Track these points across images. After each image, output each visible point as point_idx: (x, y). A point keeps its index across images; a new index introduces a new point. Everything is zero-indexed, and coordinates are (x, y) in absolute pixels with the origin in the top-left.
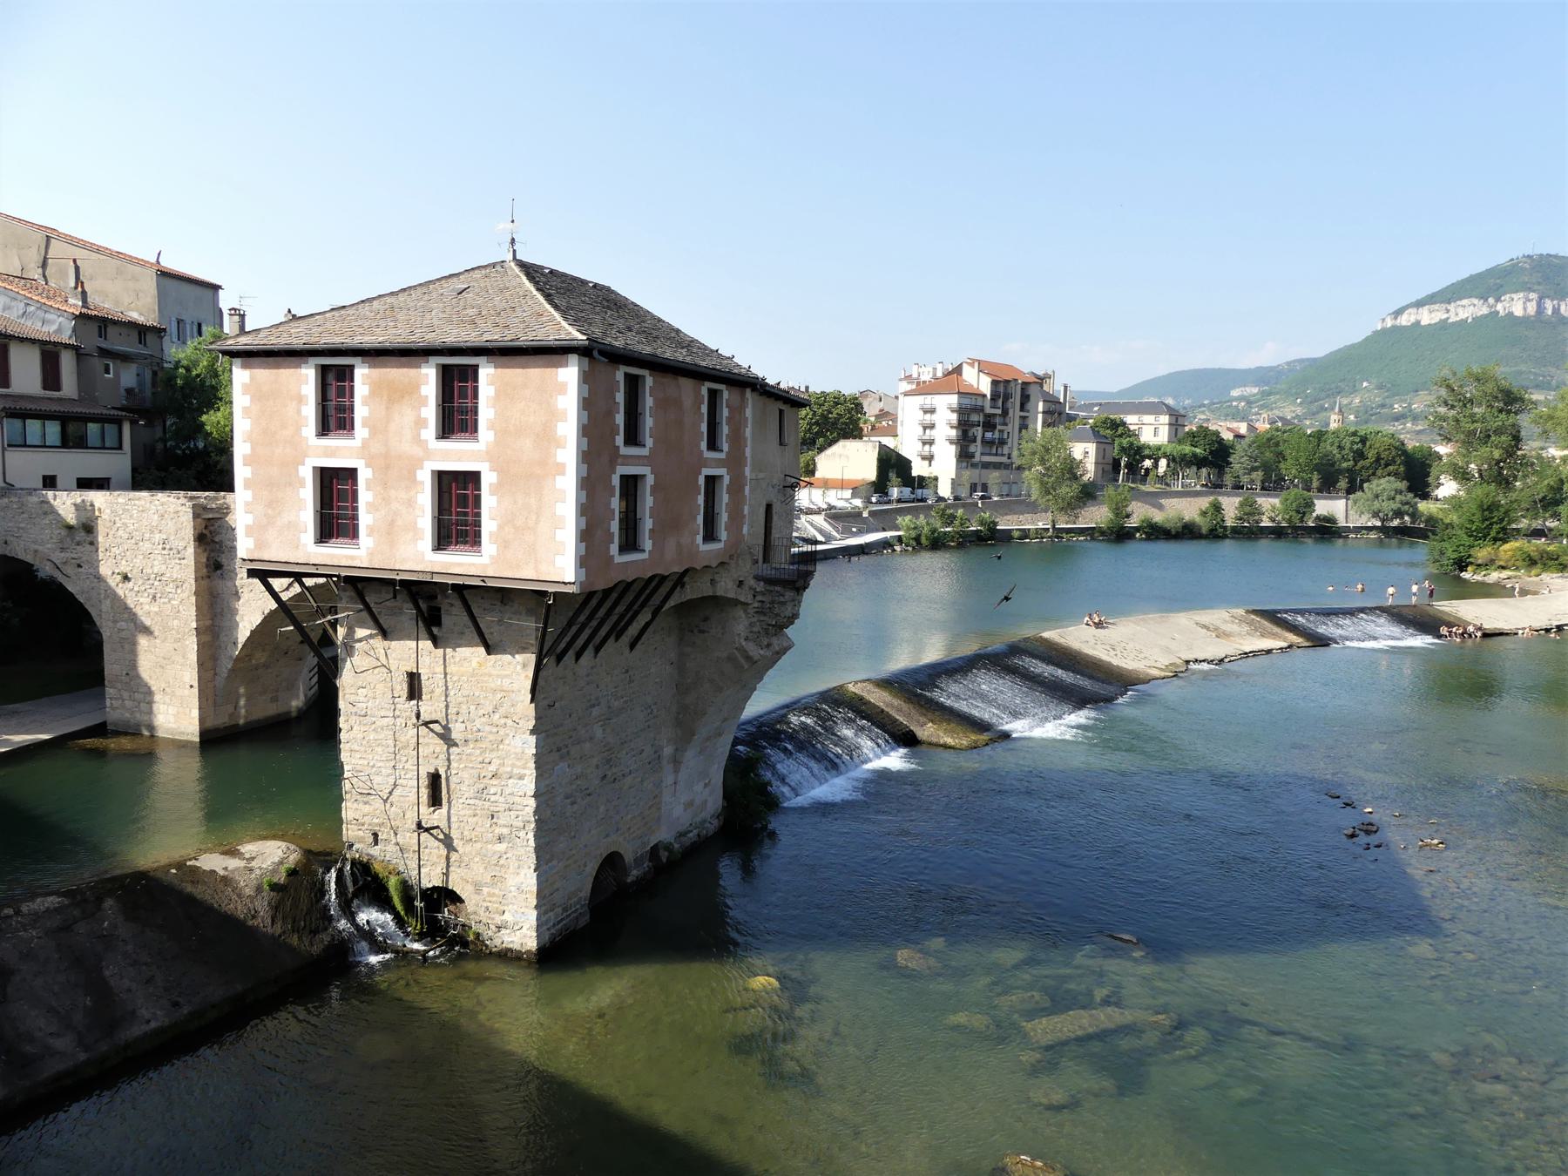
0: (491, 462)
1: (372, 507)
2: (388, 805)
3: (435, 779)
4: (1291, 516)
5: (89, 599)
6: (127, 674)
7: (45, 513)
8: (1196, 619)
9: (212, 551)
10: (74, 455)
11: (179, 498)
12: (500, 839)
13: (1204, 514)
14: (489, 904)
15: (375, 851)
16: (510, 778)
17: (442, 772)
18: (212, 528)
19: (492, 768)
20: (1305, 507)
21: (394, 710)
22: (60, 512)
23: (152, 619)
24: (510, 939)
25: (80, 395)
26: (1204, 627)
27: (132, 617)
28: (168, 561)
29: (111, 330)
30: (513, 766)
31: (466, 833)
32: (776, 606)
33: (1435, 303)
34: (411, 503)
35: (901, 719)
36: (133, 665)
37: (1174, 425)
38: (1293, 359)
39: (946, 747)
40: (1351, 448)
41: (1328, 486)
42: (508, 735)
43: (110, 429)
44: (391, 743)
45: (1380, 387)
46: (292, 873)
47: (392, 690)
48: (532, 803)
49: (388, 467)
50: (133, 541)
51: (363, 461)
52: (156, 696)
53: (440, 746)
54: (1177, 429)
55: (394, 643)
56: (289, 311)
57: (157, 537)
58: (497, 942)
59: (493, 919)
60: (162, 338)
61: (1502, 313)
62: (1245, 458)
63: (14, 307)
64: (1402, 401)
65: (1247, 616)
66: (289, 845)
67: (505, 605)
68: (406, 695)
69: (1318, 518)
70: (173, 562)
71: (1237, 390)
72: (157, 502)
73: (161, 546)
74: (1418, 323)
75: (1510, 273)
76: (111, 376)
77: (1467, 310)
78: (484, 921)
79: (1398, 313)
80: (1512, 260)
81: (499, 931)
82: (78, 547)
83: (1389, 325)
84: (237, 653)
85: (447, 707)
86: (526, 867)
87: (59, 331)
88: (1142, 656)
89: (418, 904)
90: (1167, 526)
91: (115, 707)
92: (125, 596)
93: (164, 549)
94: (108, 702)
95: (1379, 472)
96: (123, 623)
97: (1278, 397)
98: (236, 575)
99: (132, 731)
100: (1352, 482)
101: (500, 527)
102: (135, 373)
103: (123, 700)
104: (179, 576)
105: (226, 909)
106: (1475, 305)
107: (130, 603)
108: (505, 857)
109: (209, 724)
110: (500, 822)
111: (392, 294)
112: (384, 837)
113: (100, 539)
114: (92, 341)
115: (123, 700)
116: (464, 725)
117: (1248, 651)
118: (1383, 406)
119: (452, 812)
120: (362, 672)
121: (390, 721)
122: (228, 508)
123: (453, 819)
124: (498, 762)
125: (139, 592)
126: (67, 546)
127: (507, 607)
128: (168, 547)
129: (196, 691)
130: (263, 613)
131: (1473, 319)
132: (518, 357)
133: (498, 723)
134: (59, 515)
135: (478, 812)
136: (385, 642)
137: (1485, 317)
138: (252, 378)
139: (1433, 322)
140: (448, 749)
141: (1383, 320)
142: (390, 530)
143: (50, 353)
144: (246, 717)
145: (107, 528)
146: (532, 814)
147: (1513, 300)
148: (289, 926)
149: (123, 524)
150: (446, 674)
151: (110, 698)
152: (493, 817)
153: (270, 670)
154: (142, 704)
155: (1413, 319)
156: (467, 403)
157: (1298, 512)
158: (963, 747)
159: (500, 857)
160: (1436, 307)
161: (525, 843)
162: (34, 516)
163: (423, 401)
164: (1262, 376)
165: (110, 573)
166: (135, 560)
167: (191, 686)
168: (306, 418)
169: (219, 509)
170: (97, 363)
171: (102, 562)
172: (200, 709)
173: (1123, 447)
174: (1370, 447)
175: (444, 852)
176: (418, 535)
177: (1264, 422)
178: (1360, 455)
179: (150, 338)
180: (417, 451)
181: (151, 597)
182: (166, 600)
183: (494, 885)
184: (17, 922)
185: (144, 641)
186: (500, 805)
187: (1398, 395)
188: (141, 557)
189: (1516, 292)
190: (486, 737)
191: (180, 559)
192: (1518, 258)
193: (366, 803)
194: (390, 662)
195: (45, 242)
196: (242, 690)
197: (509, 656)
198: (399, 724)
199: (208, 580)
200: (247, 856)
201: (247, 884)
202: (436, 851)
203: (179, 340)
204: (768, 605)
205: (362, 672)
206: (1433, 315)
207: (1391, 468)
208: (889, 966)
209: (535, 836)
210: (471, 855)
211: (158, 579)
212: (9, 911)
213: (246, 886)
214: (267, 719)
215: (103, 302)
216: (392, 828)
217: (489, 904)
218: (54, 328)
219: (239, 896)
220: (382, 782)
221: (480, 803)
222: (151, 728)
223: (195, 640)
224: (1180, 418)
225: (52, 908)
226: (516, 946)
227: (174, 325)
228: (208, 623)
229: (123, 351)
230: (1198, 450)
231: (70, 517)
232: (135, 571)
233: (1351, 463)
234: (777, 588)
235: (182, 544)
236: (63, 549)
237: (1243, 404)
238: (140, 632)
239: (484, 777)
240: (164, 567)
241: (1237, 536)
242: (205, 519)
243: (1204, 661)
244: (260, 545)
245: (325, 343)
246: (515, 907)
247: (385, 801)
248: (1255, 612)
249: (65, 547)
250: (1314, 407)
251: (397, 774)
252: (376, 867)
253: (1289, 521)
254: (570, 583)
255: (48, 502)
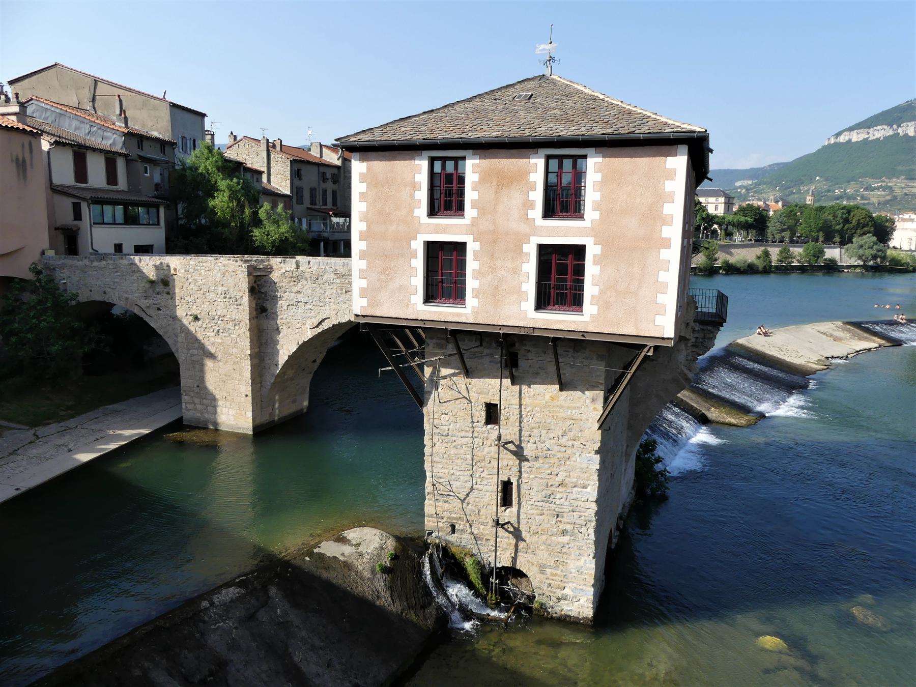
0: (594, 237)
1: (478, 274)
2: (465, 505)
3: (506, 487)
4: (810, 260)
5: (166, 333)
6: (198, 386)
7: (134, 272)
8: (817, 329)
9: (259, 299)
10: (109, 229)
11: (237, 261)
12: (563, 533)
13: (759, 258)
14: (551, 582)
15: (453, 538)
16: (575, 487)
17: (514, 481)
18: (259, 283)
19: (559, 479)
20: (819, 253)
21: (473, 432)
22: (144, 271)
23: (217, 348)
24: (569, 608)
25: (128, 188)
26: (824, 334)
27: (202, 347)
28: (228, 307)
29: (146, 144)
30: (578, 477)
31: (533, 527)
32: (706, 341)
33: (861, 128)
34: (516, 271)
35: (695, 405)
36: (202, 379)
37: (727, 203)
38: (772, 163)
39: (730, 425)
40: (841, 217)
41: (829, 239)
42: (575, 454)
43: (153, 210)
44: (469, 457)
45: (826, 180)
46: (395, 558)
47: (472, 417)
48: (594, 507)
49: (495, 242)
50: (202, 292)
51: (472, 237)
52: (219, 402)
53: (513, 461)
54: (729, 206)
55: (474, 381)
56: (232, 133)
57: (220, 289)
58: (557, 609)
59: (555, 593)
60: (174, 149)
61: (901, 134)
62: (778, 223)
63: (82, 128)
64: (840, 188)
65: (844, 326)
66: (382, 532)
67: (577, 352)
68: (484, 421)
69: (826, 260)
70: (232, 307)
71: (739, 182)
72: (220, 264)
73: (223, 296)
74: (850, 140)
75: (906, 110)
76: (148, 175)
77: (880, 132)
78: (547, 593)
79: (838, 135)
80: (908, 102)
81: (559, 602)
82: (157, 296)
83: (832, 142)
84: (278, 371)
85: (521, 430)
86: (586, 555)
87: (113, 144)
88: (799, 354)
89: (493, 580)
90: (738, 266)
91: (189, 410)
92: (196, 331)
93: (226, 298)
94: (184, 405)
95: (858, 231)
96: (194, 350)
97: (765, 186)
98: (277, 316)
99: (200, 426)
100: (842, 237)
101: (602, 292)
102: (159, 174)
103: (195, 404)
104: (237, 318)
105: (357, 591)
106: (885, 130)
107: (200, 336)
108: (567, 547)
109: (258, 422)
110: (563, 520)
111: (466, 100)
112: (461, 527)
113: (177, 290)
114: (135, 152)
115: (195, 404)
116: (535, 445)
117: (858, 350)
118: (829, 191)
119: (521, 511)
120: (445, 402)
121: (470, 440)
122: (271, 268)
123: (521, 517)
124: (565, 474)
125: (206, 328)
126: (150, 295)
127: (579, 354)
128: (228, 296)
129: (250, 398)
130: (298, 344)
131: (884, 138)
132: (664, 147)
133: (566, 444)
134: (144, 273)
135: (544, 512)
136: (467, 379)
137: (891, 136)
138: (368, 168)
139: (859, 140)
140: (520, 464)
141: (829, 139)
142: (495, 294)
143: (110, 158)
144: (279, 415)
145: (182, 283)
146: (593, 515)
147: (908, 126)
148: (405, 603)
149: (194, 279)
150: (520, 405)
151: (185, 403)
152: (558, 516)
153: (294, 381)
154: (208, 408)
155: (847, 138)
156: (452, 187)
157: (814, 256)
158: (743, 425)
159: (562, 547)
160: (861, 131)
161: (586, 537)
162: (125, 274)
163: (533, 187)
164: (753, 173)
165: (184, 315)
166: (202, 306)
167: (246, 396)
168: (419, 201)
169: (265, 269)
170: (140, 166)
171: (178, 307)
172: (253, 411)
173: (703, 217)
174: (853, 216)
175: (513, 541)
176: (522, 296)
177: (771, 201)
178: (846, 221)
179: (167, 149)
180: (523, 228)
181: (215, 332)
182: (227, 334)
183: (556, 567)
184: (215, 613)
185: (210, 363)
186: (565, 507)
187: (837, 184)
188: (208, 303)
189: (910, 121)
190: (554, 455)
191: (237, 305)
192: (911, 101)
193: (446, 502)
194: (471, 395)
195: (93, 84)
196: (277, 397)
197: (579, 393)
198: (476, 443)
199: (256, 320)
200: (354, 543)
201: (363, 566)
202: (506, 540)
203: (183, 150)
204: (701, 340)
205: (445, 402)
206: (859, 136)
207: (866, 229)
208: (847, 621)
209: (595, 532)
210: (537, 544)
211: (221, 319)
212: (205, 604)
213: (363, 569)
214: (291, 415)
215: (134, 125)
216: (468, 521)
217: (551, 582)
218: (110, 142)
219: (361, 578)
220: (461, 486)
221: (547, 505)
222: (216, 424)
223: (250, 363)
224: (731, 199)
225: (234, 598)
226: (573, 614)
227: (180, 140)
228: (257, 350)
229: (155, 158)
230: (749, 219)
231: (152, 274)
232: (203, 314)
233: (841, 226)
234: (709, 328)
235: (239, 295)
236: (146, 298)
237: (744, 190)
238: (207, 357)
239: (551, 485)
240: (225, 311)
241: (779, 271)
242: (254, 276)
243: (837, 357)
244: (371, 304)
245: (443, 138)
246: (574, 585)
247: (463, 501)
248: (848, 323)
249: (148, 295)
250: (787, 192)
251: (474, 481)
252: (453, 550)
253: (809, 262)
254: (668, 339)
255: (135, 264)
